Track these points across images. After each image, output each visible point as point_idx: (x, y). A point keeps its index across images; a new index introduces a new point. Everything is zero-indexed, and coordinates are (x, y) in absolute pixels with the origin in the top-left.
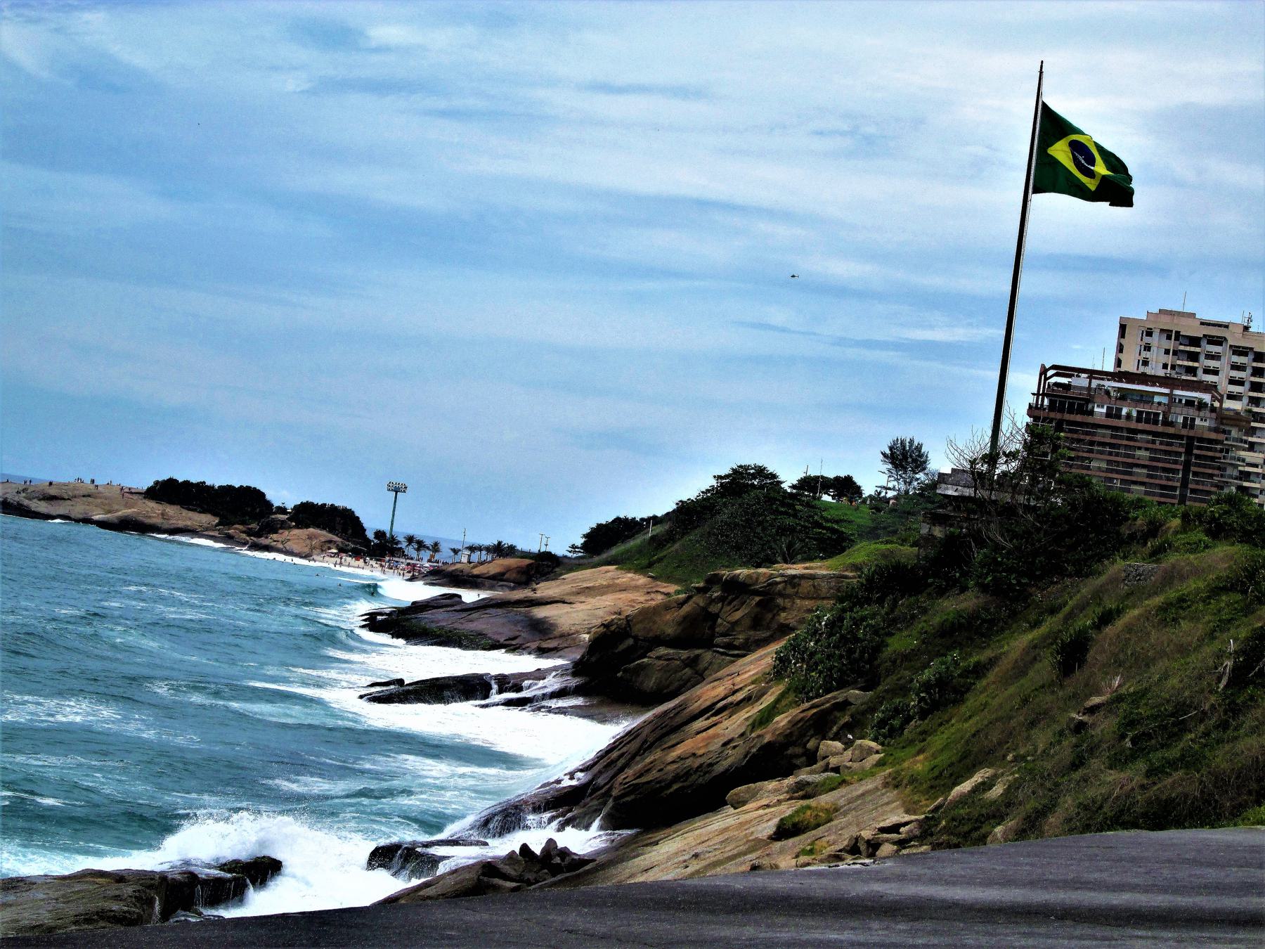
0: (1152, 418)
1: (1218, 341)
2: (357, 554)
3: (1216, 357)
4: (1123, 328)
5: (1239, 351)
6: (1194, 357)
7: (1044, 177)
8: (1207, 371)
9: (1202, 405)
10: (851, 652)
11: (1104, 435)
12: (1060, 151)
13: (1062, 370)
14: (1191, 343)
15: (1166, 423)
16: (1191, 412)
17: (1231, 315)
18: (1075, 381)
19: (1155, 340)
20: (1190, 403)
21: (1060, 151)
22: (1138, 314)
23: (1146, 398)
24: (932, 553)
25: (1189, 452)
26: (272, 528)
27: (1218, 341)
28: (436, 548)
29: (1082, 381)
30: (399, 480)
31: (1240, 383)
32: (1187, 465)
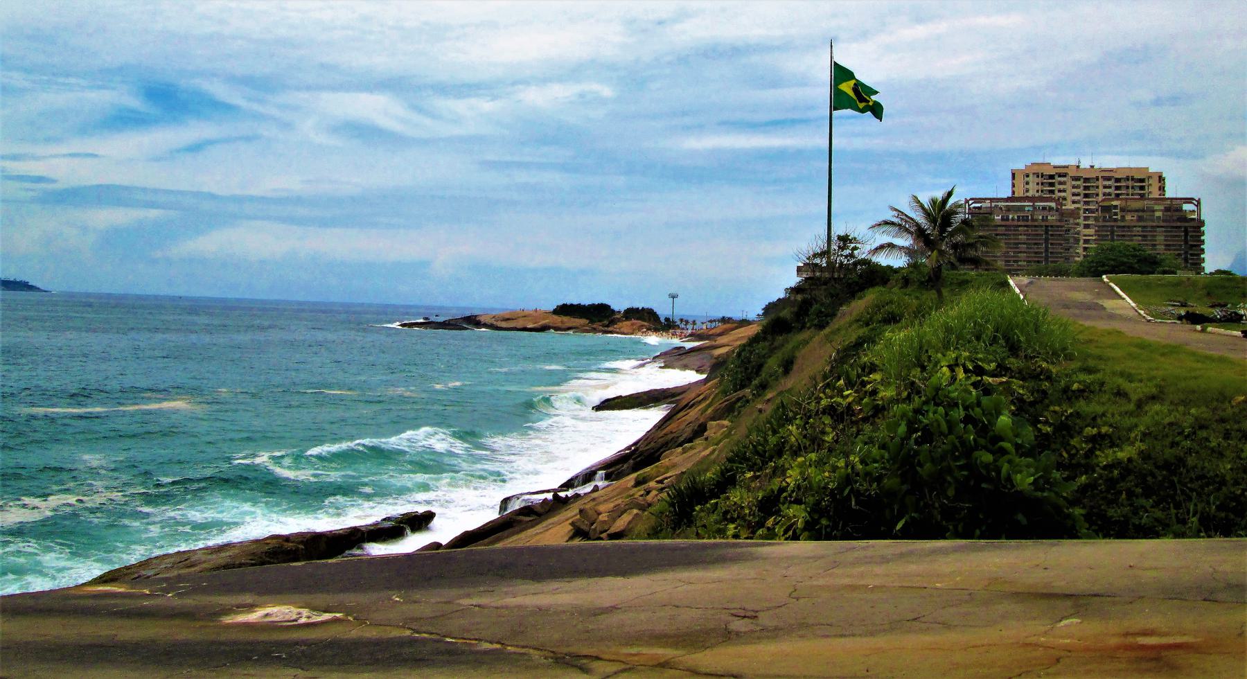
0: (1025, 219)
1: (1064, 175)
2: (656, 330)
3: (1064, 183)
4: (1013, 175)
5: (1076, 179)
6: (1052, 185)
7: (838, 101)
8: (1060, 191)
9: (1051, 209)
10: (747, 369)
11: (1001, 230)
12: (846, 87)
13: (976, 200)
14: (1051, 178)
15: (1033, 220)
16: (1046, 213)
17: (1071, 161)
18: (984, 205)
19: (1031, 178)
20: (1044, 208)
21: (846, 87)
22: (1020, 166)
23: (1021, 209)
24: (796, 309)
25: (1046, 233)
26: (613, 322)
27: (1064, 175)
28: (694, 323)
29: (987, 204)
30: (673, 291)
31: (1078, 195)
32: (1046, 240)
